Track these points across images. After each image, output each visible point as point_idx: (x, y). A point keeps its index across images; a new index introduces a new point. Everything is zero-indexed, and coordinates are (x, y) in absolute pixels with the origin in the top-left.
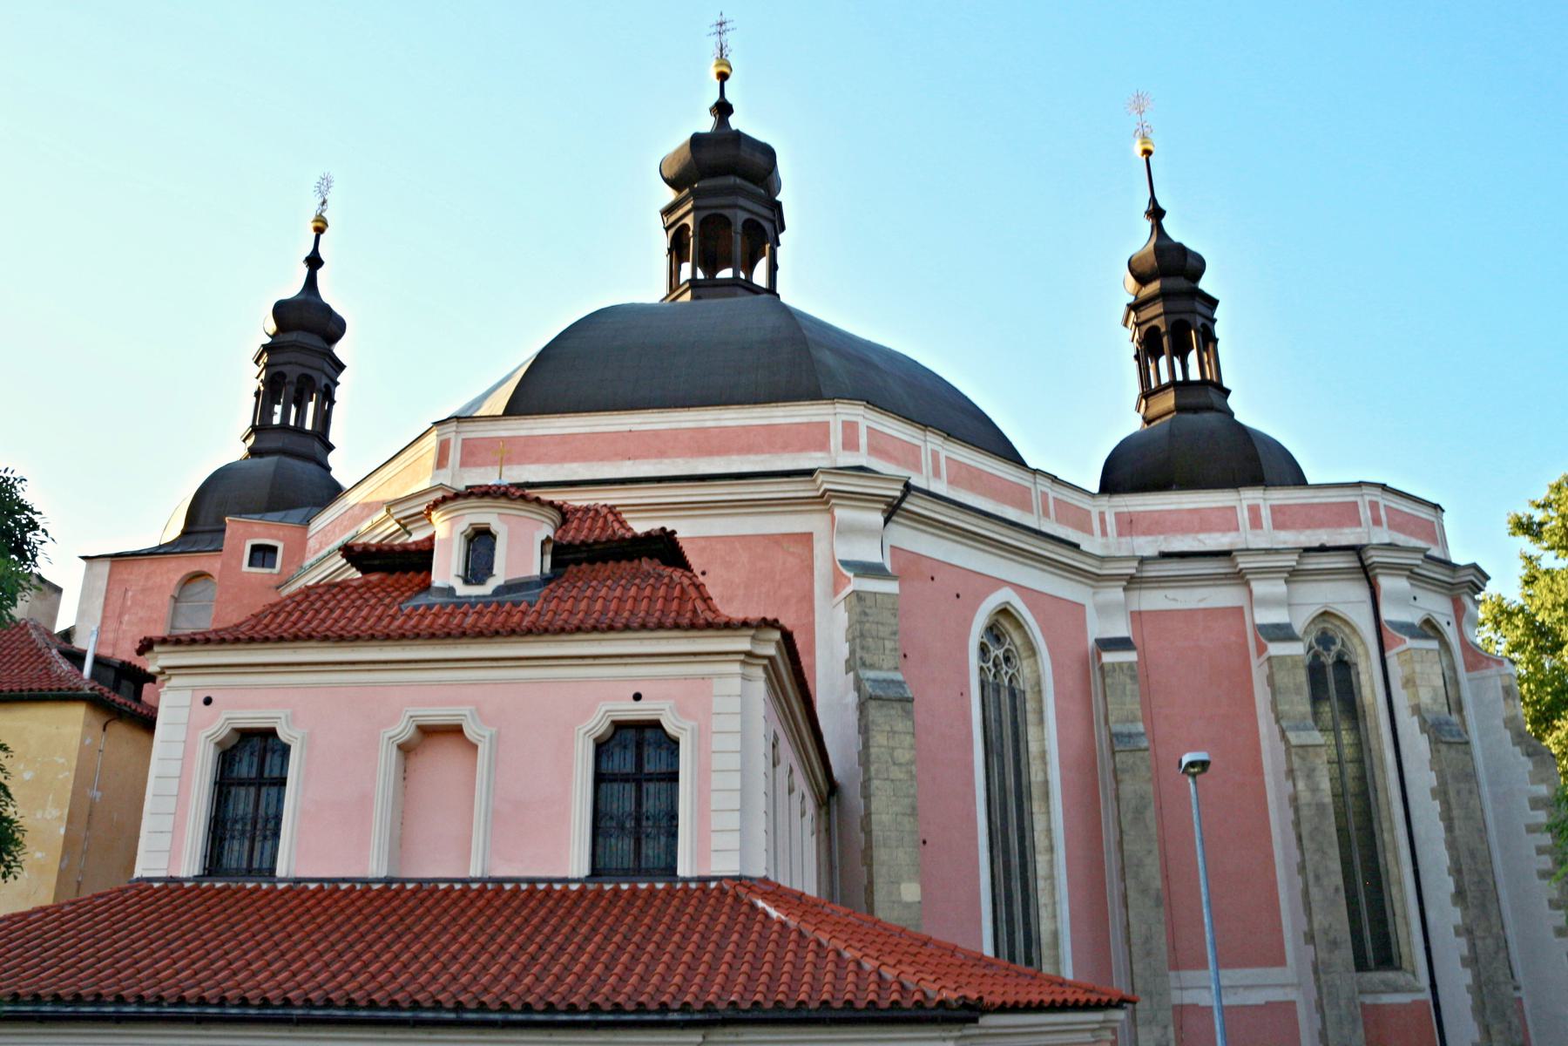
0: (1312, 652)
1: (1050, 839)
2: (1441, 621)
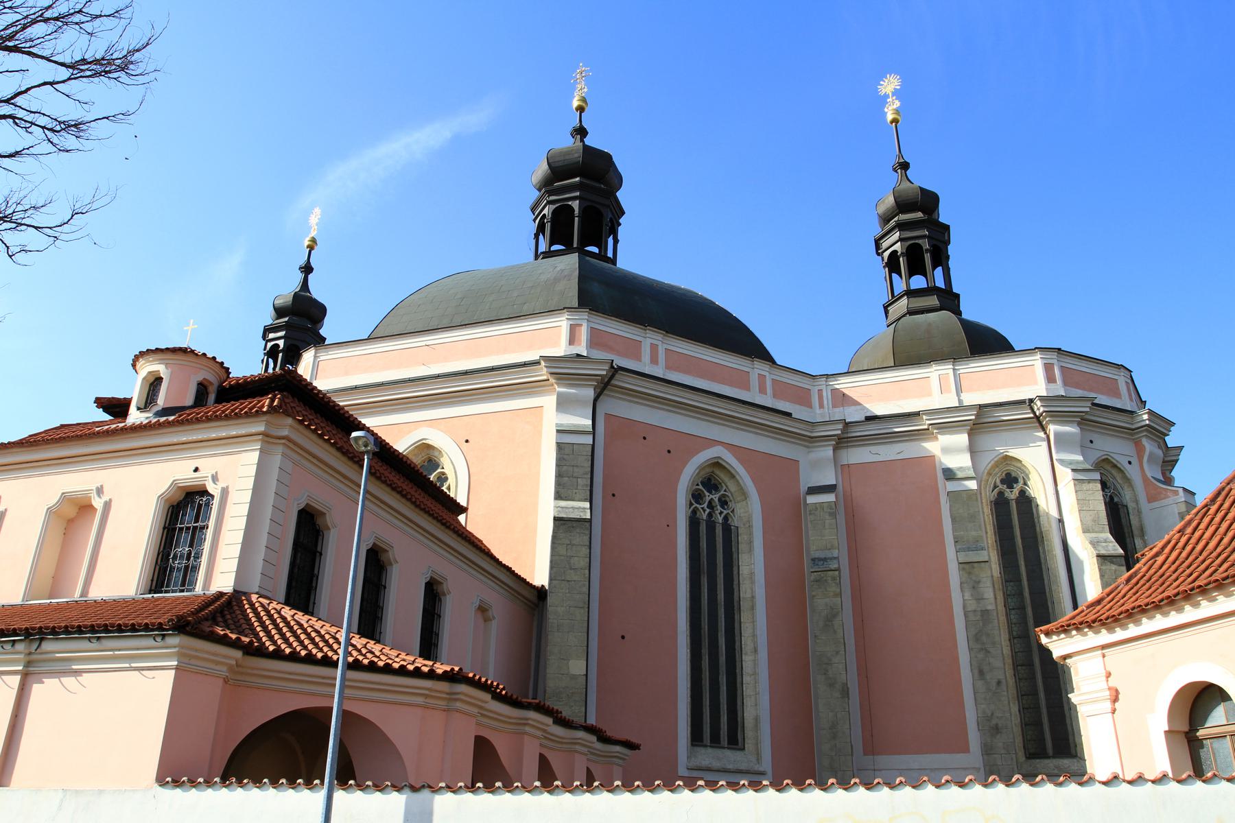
1: (755, 643)
2: (1123, 462)
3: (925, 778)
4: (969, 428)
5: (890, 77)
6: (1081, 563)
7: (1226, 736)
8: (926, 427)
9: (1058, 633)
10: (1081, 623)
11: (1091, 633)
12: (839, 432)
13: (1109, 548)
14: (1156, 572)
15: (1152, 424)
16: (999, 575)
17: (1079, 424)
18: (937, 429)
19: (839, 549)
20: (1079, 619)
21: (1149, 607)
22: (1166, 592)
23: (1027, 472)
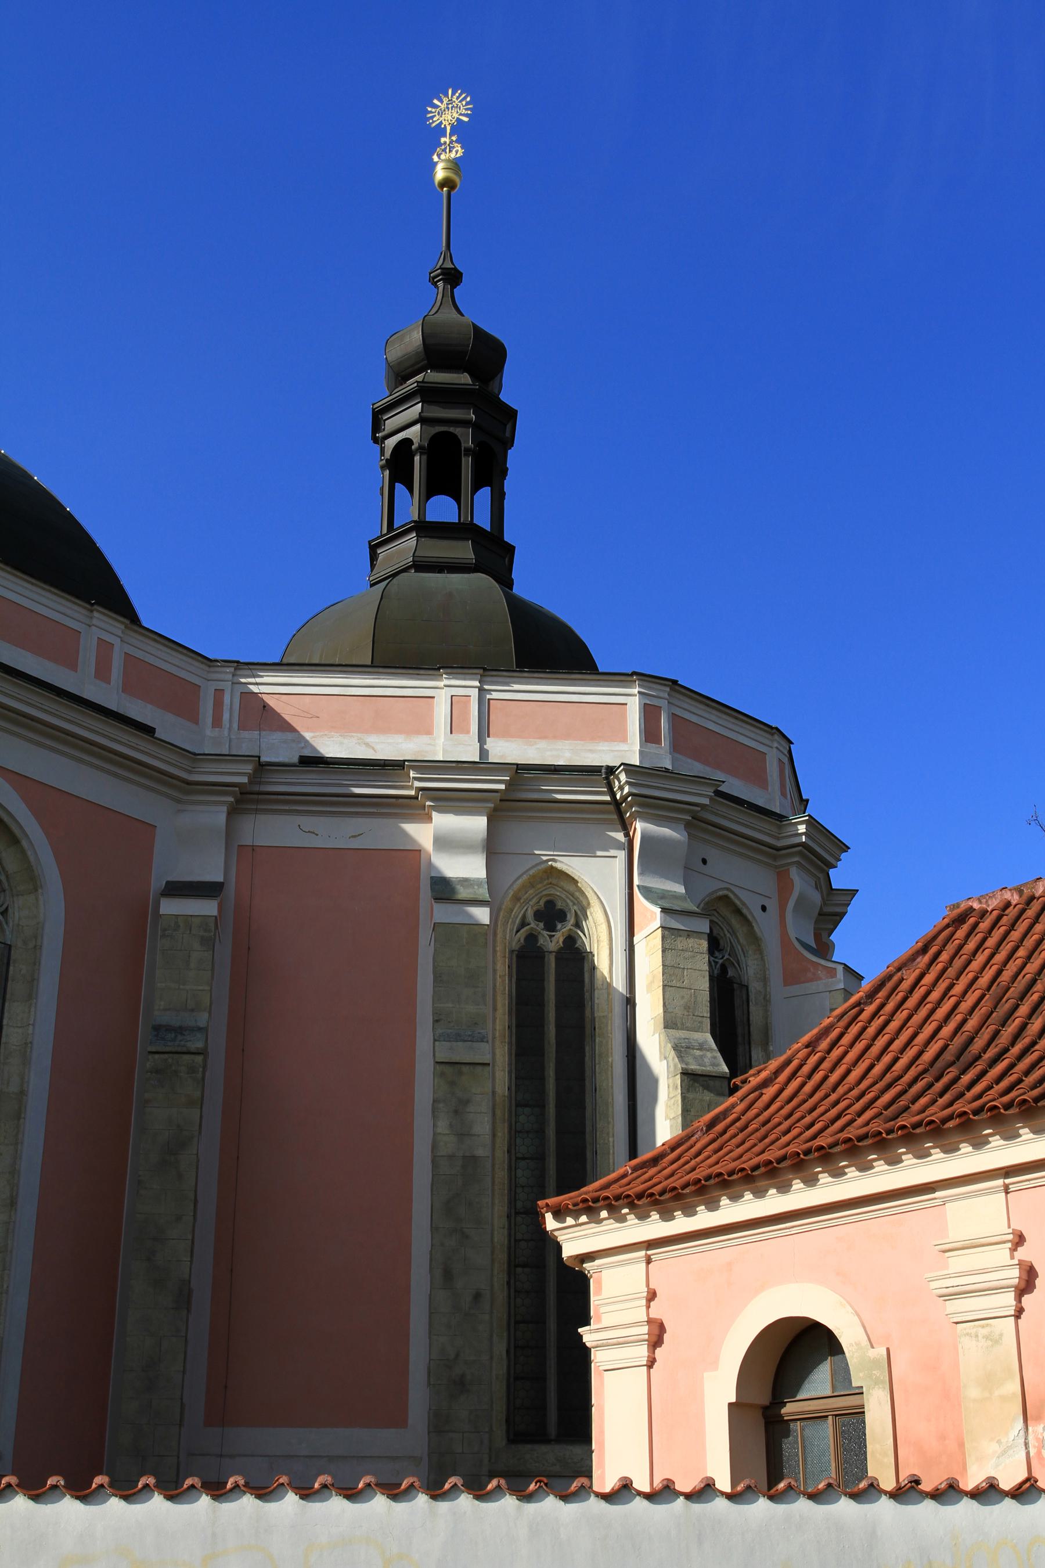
0: (524, 931)
2: (752, 905)
3: (284, 1479)
4: (492, 805)
5: (453, 94)
6: (654, 1081)
7: (827, 1416)
8: (413, 793)
9: (576, 1215)
10: (617, 1198)
11: (632, 1216)
12: (244, 780)
13: (706, 1060)
14: (757, 1115)
15: (810, 843)
16: (506, 1093)
17: (688, 826)
18: (432, 800)
19: (210, 1013)
20: (615, 1189)
21: (735, 1177)
22: (766, 1153)
23: (585, 903)
